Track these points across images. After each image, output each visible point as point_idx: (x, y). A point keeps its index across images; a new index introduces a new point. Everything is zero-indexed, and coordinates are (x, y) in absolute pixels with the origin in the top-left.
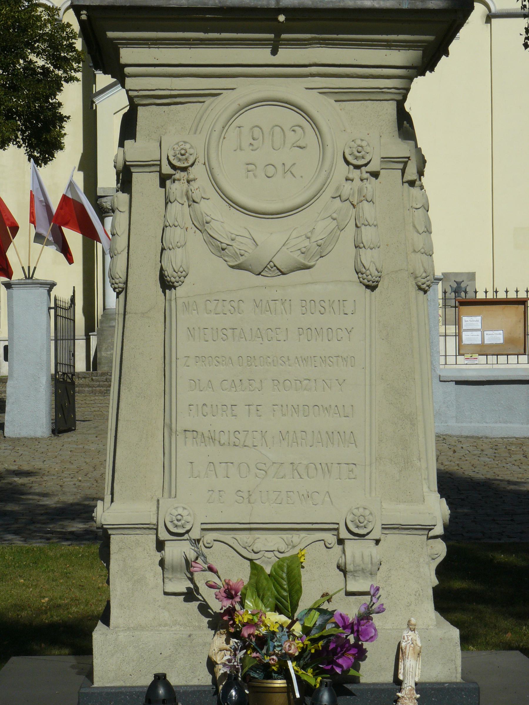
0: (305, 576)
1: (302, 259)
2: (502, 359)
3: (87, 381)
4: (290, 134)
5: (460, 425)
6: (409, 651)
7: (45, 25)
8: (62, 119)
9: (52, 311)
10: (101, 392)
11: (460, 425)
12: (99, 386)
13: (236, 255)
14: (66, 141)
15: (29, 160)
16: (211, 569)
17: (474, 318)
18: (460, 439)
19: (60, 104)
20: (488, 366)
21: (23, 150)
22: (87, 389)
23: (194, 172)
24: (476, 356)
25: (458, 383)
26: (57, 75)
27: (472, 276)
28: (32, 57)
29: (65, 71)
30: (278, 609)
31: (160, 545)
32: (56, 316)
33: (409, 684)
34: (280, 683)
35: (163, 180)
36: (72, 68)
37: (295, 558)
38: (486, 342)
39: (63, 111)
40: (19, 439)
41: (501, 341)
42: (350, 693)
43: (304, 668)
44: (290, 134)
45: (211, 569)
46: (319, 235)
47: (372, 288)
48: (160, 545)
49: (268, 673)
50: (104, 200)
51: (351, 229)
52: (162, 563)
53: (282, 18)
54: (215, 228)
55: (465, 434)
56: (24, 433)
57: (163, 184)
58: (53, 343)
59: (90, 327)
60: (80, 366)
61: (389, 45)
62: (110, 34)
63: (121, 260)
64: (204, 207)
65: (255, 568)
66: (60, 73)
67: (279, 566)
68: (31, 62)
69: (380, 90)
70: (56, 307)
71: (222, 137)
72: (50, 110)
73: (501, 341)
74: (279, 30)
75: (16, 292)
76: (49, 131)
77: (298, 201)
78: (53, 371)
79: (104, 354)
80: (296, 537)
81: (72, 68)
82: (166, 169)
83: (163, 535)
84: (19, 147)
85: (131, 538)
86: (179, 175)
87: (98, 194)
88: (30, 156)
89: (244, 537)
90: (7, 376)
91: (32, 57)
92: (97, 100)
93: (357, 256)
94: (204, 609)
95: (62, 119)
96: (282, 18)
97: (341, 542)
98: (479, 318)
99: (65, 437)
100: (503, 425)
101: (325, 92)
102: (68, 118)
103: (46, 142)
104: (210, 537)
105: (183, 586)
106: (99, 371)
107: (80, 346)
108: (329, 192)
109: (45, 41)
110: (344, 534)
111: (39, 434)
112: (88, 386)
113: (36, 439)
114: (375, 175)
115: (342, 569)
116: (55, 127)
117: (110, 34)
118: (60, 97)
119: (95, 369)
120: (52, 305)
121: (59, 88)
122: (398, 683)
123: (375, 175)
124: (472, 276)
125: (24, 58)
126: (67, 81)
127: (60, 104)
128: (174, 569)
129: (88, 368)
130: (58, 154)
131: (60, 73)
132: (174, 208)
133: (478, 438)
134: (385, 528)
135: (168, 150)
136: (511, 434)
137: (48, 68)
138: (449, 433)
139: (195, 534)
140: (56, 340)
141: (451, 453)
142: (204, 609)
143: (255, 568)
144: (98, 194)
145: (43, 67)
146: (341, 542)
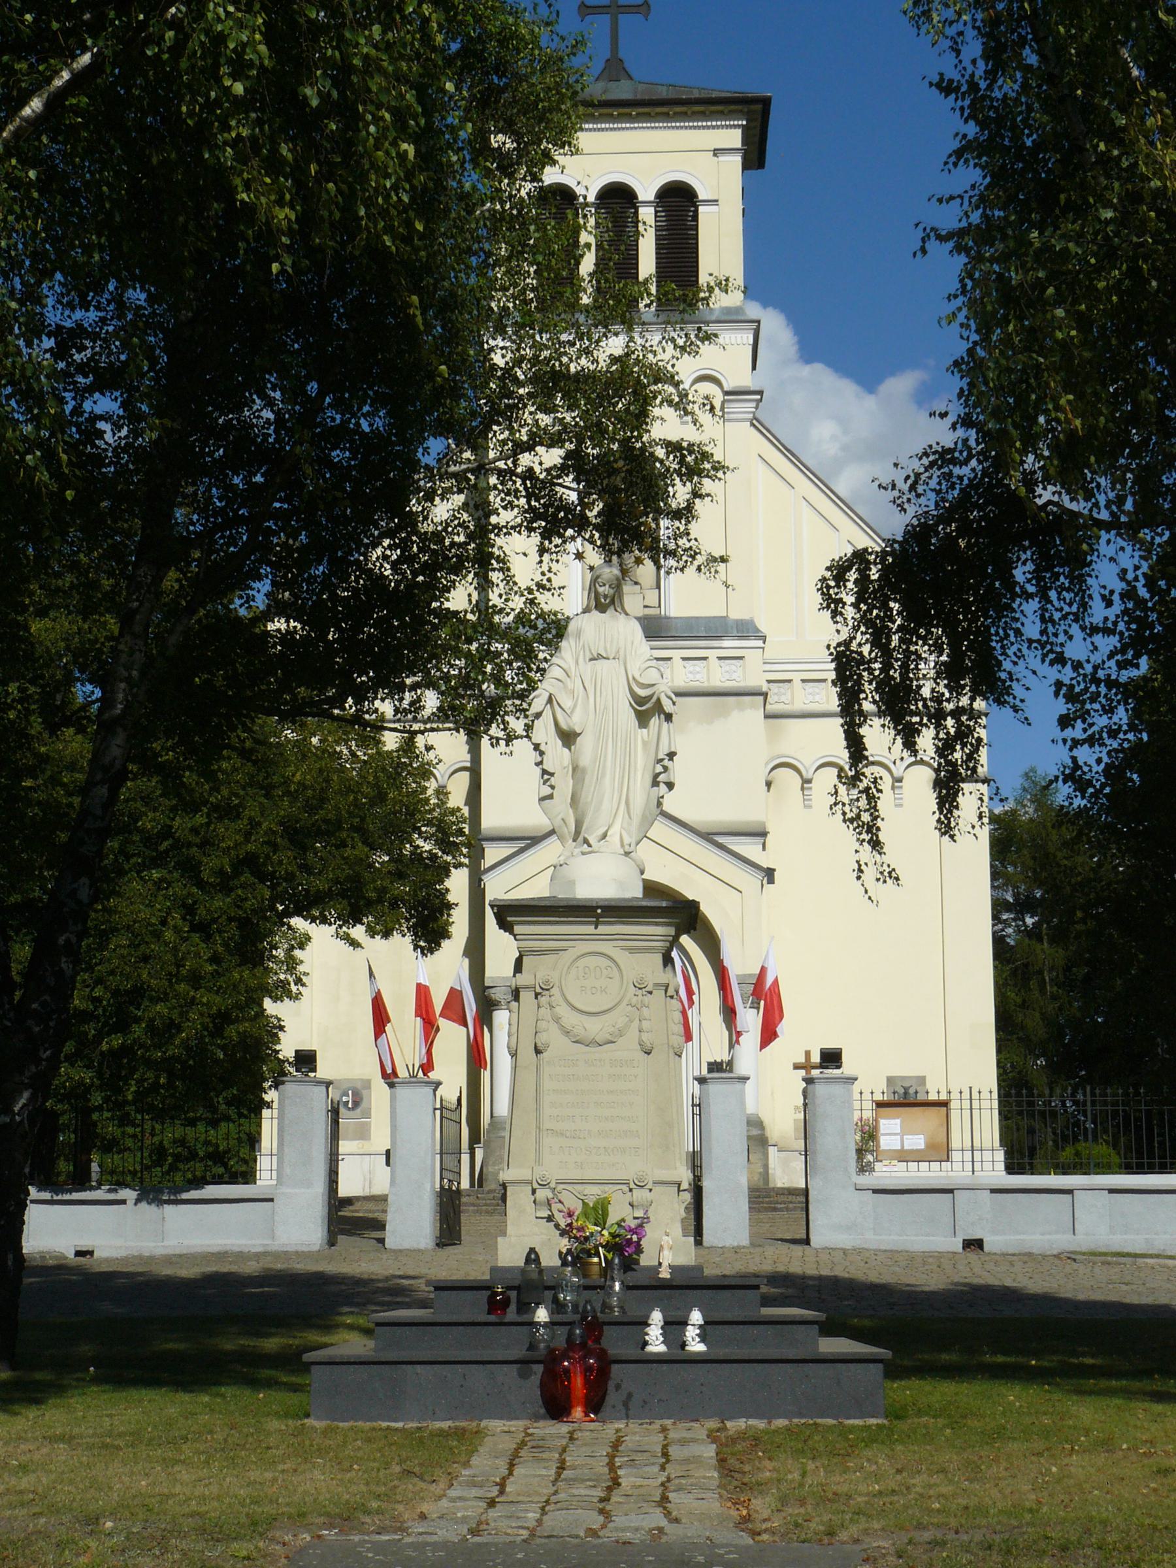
0: (610, 1208)
1: (610, 1038)
2: (924, 1166)
3: (472, 1199)
4: (604, 971)
5: (877, 1237)
6: (665, 1247)
7: (434, 810)
8: (449, 906)
9: (438, 1112)
10: (487, 1212)
11: (877, 1237)
12: (486, 1205)
13: (575, 1036)
14: (452, 929)
15: (415, 949)
16: (560, 1202)
17: (893, 1121)
18: (876, 1252)
19: (447, 890)
20: (907, 1174)
21: (408, 939)
22: (471, 1208)
23: (553, 991)
24: (895, 1162)
25: (875, 1191)
26: (446, 861)
27: (922, 1080)
28: (420, 842)
29: (454, 857)
30: (596, 1225)
31: (534, 1192)
32: (442, 1117)
33: (665, 1264)
34: (596, 1260)
35: (537, 995)
36: (462, 854)
37: (605, 1198)
38: (906, 1148)
39: (451, 898)
40: (401, 1251)
41: (923, 1147)
42: (634, 1270)
43: (609, 1252)
44: (604, 971)
45: (560, 1202)
46: (619, 1025)
47: (649, 1054)
48: (534, 1192)
49: (590, 1256)
50: (493, 991)
51: (637, 1022)
52: (535, 1202)
53: (599, 911)
54: (564, 1022)
55: (883, 1247)
56: (407, 1244)
57: (536, 998)
58: (438, 1156)
59: (475, 1138)
60: (465, 1184)
61: (657, 924)
62: (509, 919)
63: (514, 1039)
64: (558, 1009)
65: (585, 1204)
66: (449, 858)
67: (597, 1203)
68: (418, 847)
69: (653, 948)
70: (442, 1108)
71: (568, 972)
72: (438, 897)
73: (923, 1147)
74: (598, 916)
75: (400, 1091)
76: (436, 919)
77: (609, 1006)
78: (438, 1186)
79: (490, 1169)
80: (606, 1188)
81: (462, 854)
82: (538, 990)
83: (535, 1186)
84: (404, 936)
85: (517, 1188)
86: (545, 993)
87: (486, 984)
88: (416, 947)
89: (579, 1187)
90: (383, 1199)
91: (420, 842)
92: (486, 878)
93: (640, 1037)
94: (557, 1226)
95: (449, 906)
96: (599, 911)
97: (631, 1190)
98: (898, 1121)
99: (450, 1250)
100: (924, 1238)
101: (623, 949)
102: (457, 905)
103: (433, 930)
104: (561, 1187)
105: (546, 1213)
106: (486, 1188)
107: (465, 1158)
108: (625, 1002)
109: (433, 825)
110: (632, 1186)
111: (422, 1246)
112: (473, 1205)
113: (419, 1250)
114: (650, 993)
115: (631, 1205)
116: (442, 915)
117: (509, 919)
118: (448, 883)
119: (480, 1185)
120: (438, 1106)
121: (448, 874)
122: (660, 1264)
123: (650, 993)
124: (922, 1080)
125: (411, 843)
126: (456, 867)
127: (447, 890)
128: (541, 1204)
129: (472, 1184)
130: (445, 944)
131: (449, 858)
132: (542, 1010)
133: (897, 1252)
134: (654, 1183)
135: (539, 980)
136: (933, 1248)
137: (436, 854)
138: (866, 1246)
139: (553, 1185)
140: (441, 1154)
141: (862, 1264)
142: (557, 1226)
143: (585, 1204)
144: (486, 984)
145: (430, 851)
146: (631, 1190)
